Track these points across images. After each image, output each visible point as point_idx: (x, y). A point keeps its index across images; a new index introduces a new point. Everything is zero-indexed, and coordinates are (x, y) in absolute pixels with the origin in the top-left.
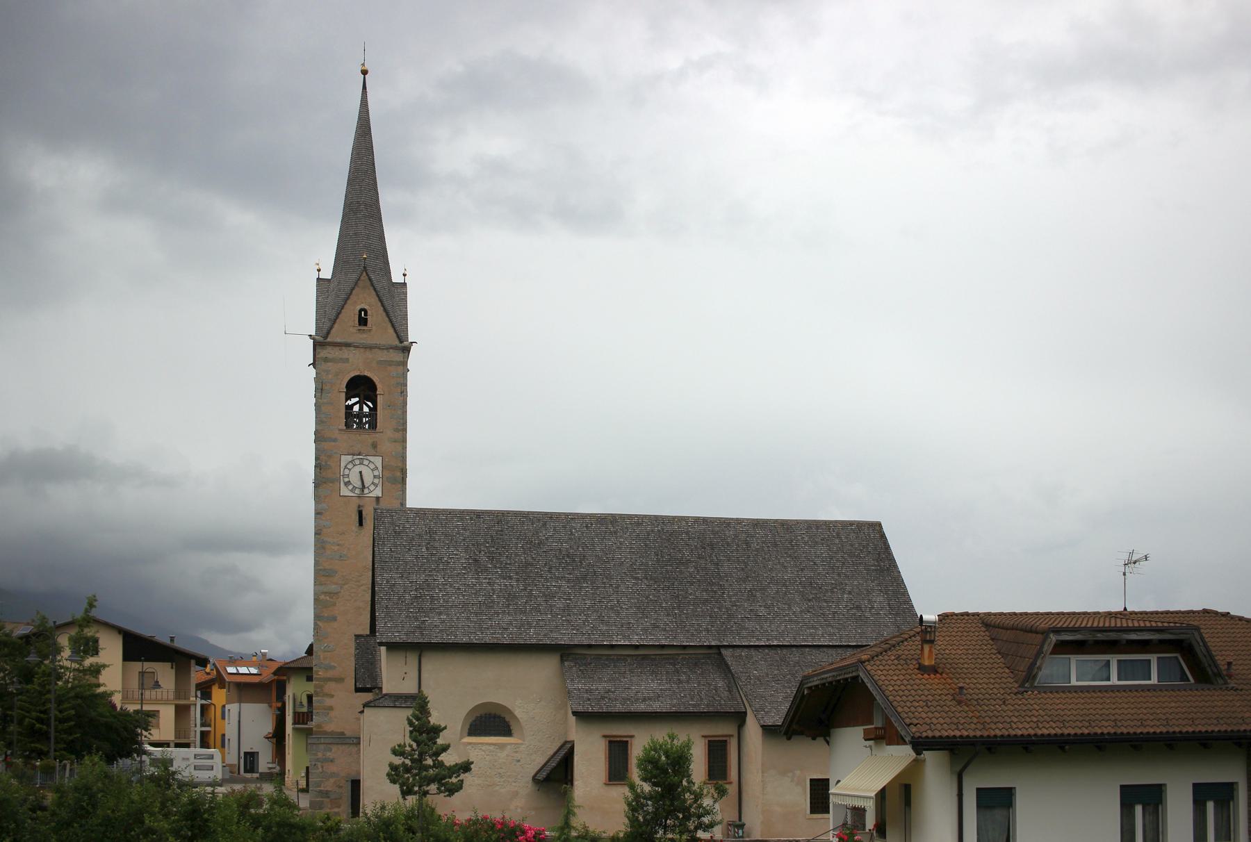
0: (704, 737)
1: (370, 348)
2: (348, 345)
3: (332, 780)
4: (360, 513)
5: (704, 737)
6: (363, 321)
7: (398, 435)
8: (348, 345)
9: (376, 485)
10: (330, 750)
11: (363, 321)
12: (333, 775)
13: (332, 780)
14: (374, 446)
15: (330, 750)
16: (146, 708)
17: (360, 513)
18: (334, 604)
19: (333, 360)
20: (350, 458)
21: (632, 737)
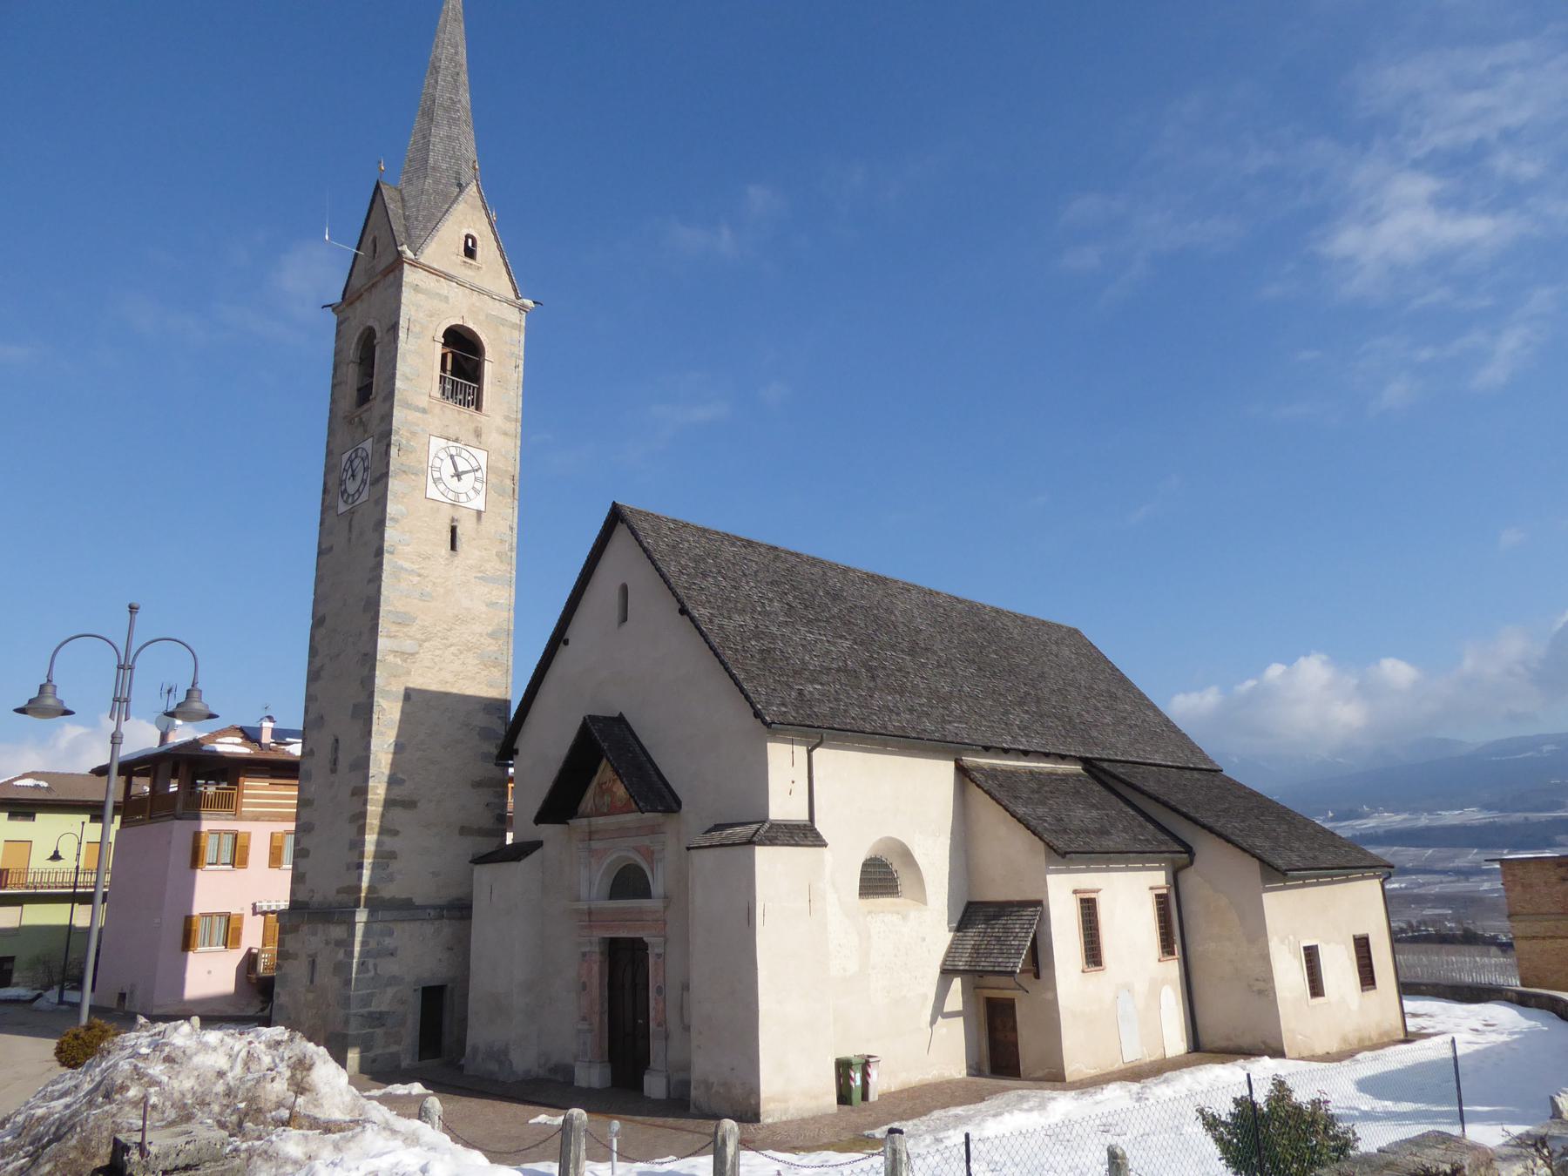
0: (1075, 892)
1: (481, 291)
2: (448, 277)
3: (390, 991)
4: (453, 530)
5: (1075, 892)
6: (470, 252)
7: (305, 843)
8: (448, 277)
9: (477, 492)
10: (391, 933)
11: (470, 252)
12: (393, 980)
13: (390, 991)
14: (478, 434)
15: (391, 933)
16: (361, 916)
17: (453, 530)
18: (408, 673)
19: (426, 292)
20: (443, 443)
21: (1098, 891)
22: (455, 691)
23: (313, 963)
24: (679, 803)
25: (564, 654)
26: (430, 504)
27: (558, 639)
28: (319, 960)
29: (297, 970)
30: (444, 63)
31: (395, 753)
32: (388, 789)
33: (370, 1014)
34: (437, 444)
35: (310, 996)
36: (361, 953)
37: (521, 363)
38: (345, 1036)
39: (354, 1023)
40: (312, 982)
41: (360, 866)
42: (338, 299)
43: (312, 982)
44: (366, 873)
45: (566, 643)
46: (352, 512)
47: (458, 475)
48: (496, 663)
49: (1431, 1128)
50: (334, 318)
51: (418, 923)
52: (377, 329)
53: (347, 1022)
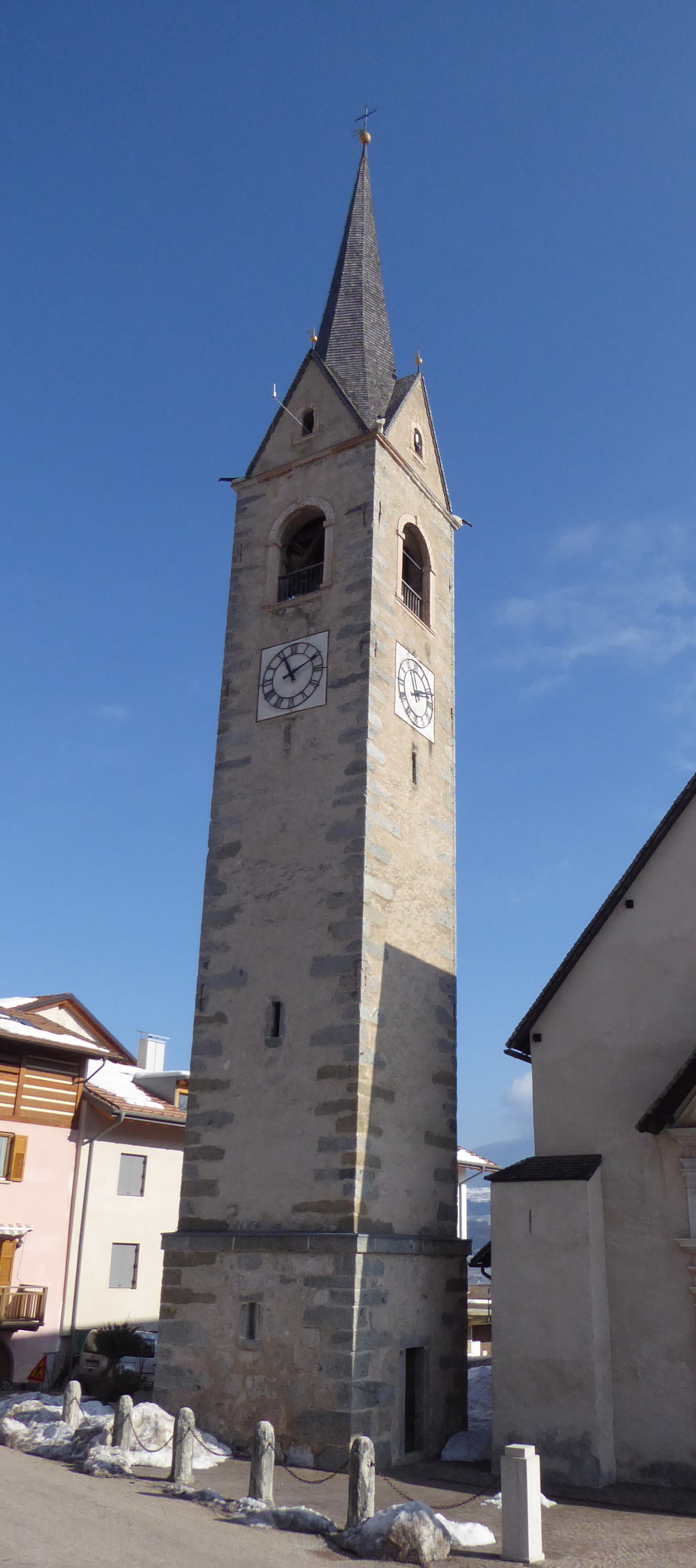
16: (362, 1244)
17: (414, 756)
22: (418, 955)
23: (252, 1309)
24: (319, 1142)
25: (622, 917)
26: (398, 722)
27: (619, 898)
28: (266, 1304)
29: (219, 1320)
30: (365, 253)
31: (379, 1026)
32: (375, 1073)
33: (368, 1384)
34: (402, 653)
35: (247, 1357)
36: (363, 1296)
37: (453, 583)
38: (347, 1416)
39: (356, 1396)
40: (251, 1334)
41: (351, 1174)
42: (241, 473)
43: (251, 1334)
44: (358, 1184)
45: (630, 904)
46: (290, 720)
47: (417, 694)
48: (446, 931)
49: (288, 1508)
50: (230, 497)
51: (402, 1257)
52: (330, 515)
53: (344, 1395)
